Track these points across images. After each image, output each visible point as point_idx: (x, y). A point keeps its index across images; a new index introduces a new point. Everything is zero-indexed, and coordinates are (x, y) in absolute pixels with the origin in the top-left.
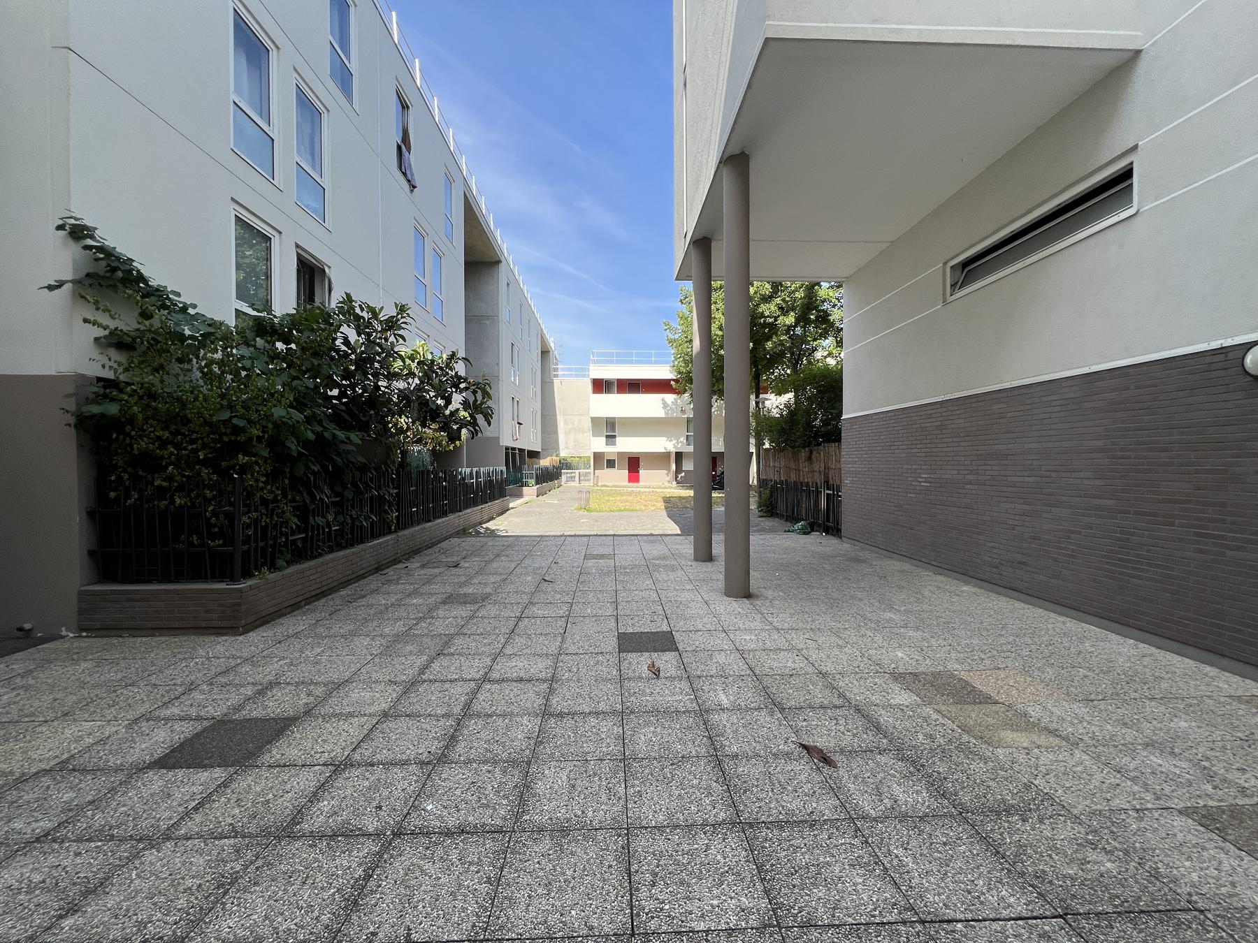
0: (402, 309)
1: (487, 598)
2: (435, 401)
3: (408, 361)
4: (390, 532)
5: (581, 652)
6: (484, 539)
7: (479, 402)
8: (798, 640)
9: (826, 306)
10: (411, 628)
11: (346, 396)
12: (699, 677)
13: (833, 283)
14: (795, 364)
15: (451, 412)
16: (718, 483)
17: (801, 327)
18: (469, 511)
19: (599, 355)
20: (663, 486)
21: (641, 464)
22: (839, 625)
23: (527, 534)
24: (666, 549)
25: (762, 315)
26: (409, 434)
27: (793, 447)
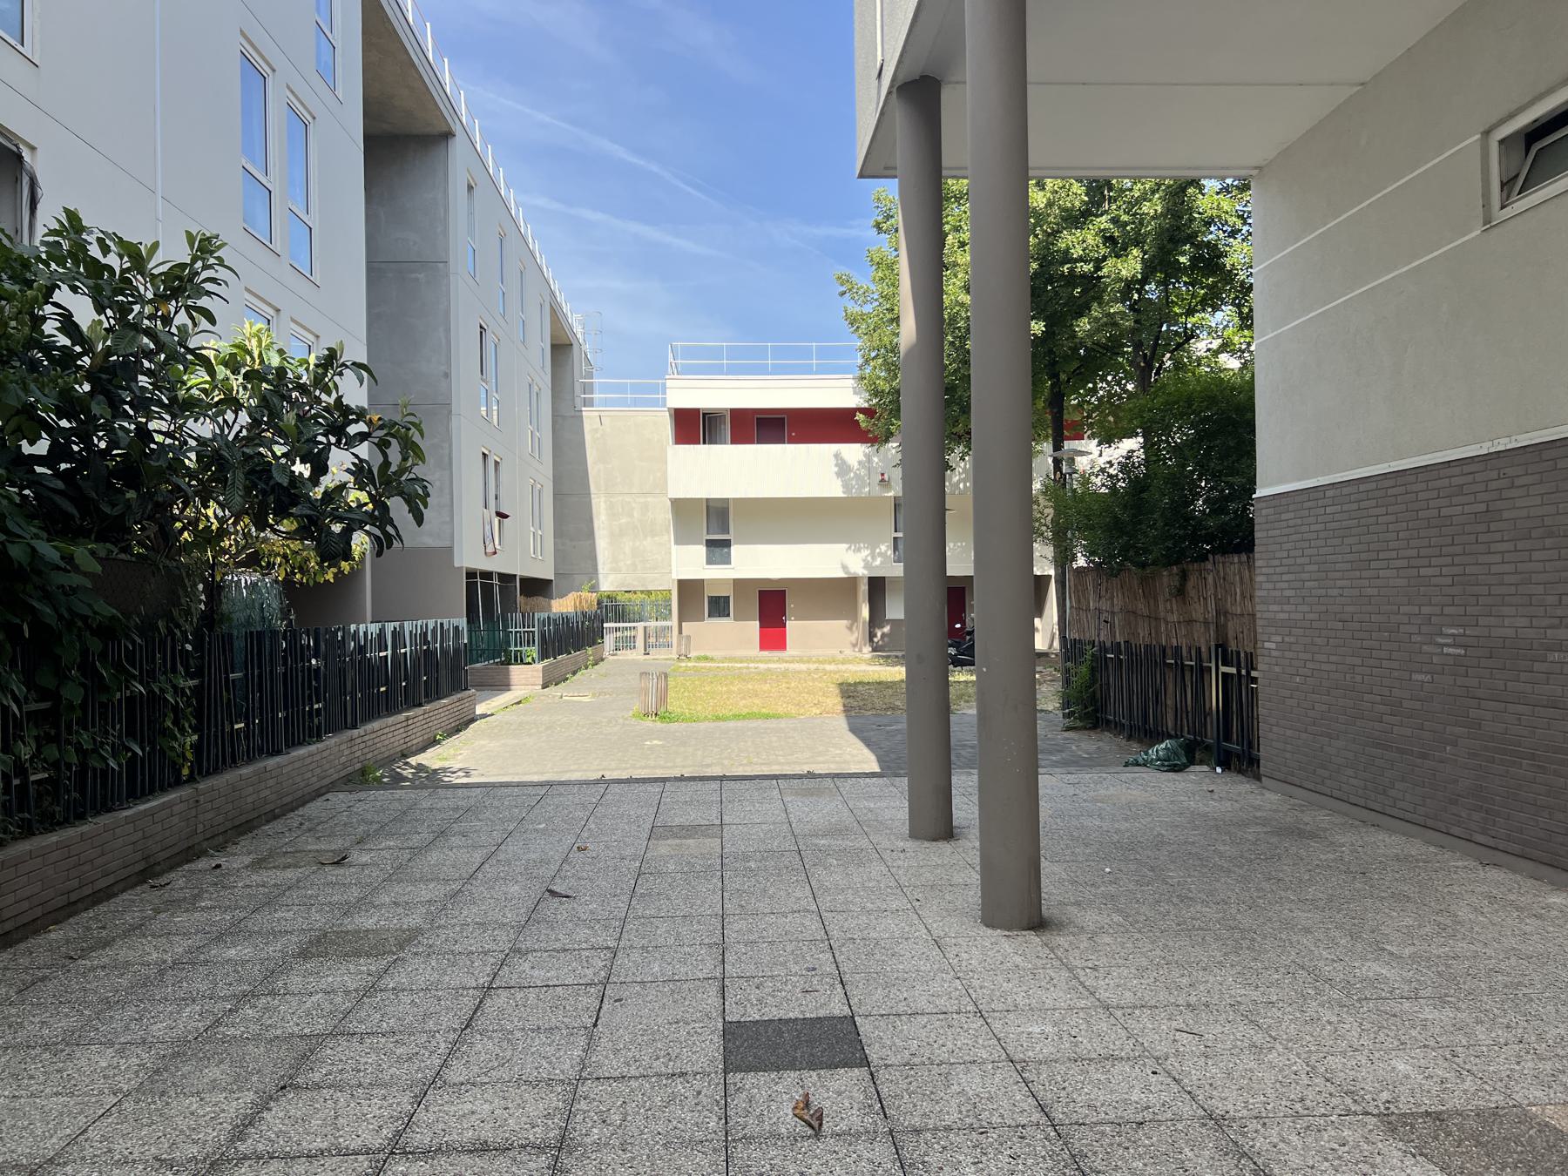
0: (205, 247)
1: (409, 940)
2: (285, 467)
3: (222, 372)
4: (178, 782)
5: (633, 1072)
6: (412, 794)
7: (393, 468)
8: (1156, 1033)
9: (1213, 235)
10: (218, 1022)
11: (69, 456)
12: (917, 1131)
13: (1229, 181)
14: (1145, 369)
15: (325, 493)
16: (962, 649)
17: (1158, 284)
18: (376, 725)
19: (688, 353)
20: (840, 657)
21: (790, 606)
22: (1255, 995)
23: (516, 779)
24: (846, 810)
25: (1066, 257)
26: (226, 543)
27: (1143, 566)
